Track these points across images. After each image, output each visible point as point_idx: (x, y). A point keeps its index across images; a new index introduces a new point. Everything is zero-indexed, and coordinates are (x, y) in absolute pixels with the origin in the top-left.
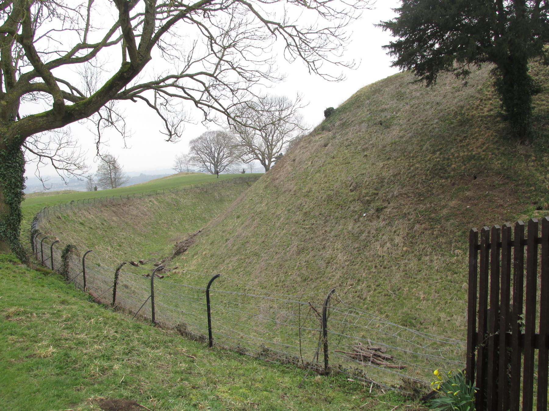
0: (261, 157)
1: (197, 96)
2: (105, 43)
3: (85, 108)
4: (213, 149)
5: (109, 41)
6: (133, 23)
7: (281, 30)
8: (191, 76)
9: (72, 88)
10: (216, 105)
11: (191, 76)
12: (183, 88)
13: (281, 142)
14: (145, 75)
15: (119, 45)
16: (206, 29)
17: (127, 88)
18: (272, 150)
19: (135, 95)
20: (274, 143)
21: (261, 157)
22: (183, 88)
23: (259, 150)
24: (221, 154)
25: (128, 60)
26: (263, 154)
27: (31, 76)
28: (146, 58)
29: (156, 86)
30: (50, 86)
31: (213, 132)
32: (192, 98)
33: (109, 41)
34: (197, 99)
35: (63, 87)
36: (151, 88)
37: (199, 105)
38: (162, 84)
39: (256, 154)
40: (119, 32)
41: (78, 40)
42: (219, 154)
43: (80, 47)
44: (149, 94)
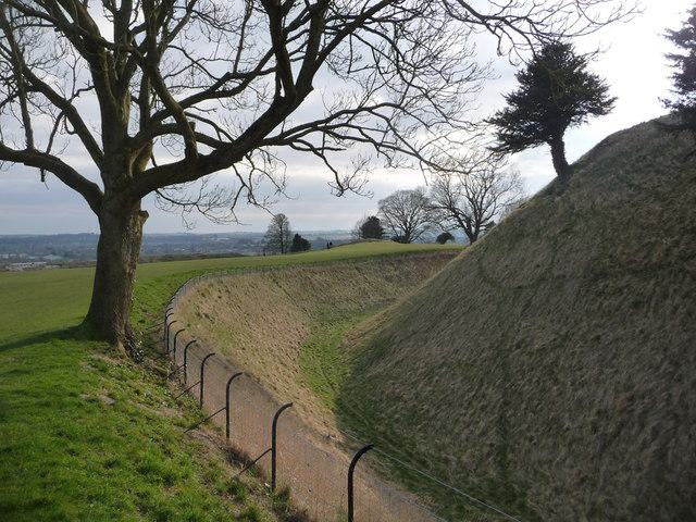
0: (465, 224)
1: (378, 137)
2: (258, 72)
3: (229, 153)
4: (406, 212)
5: (263, 70)
6: (290, 47)
7: (507, 28)
8: (370, 110)
9: (218, 130)
10: (406, 148)
11: (370, 110)
12: (360, 129)
13: (493, 205)
14: (310, 109)
15: (273, 74)
16: (299, 149)
17: (287, 129)
18: (481, 215)
19: (295, 139)
20: (484, 207)
21: (465, 224)
22: (360, 129)
23: (463, 215)
24: (415, 218)
25: (283, 94)
26: (469, 220)
27: (161, 115)
28: (305, 86)
29: (323, 126)
30: (184, 128)
31: (407, 192)
32: (370, 140)
33: (263, 70)
34: (378, 141)
35: (200, 128)
36: (316, 129)
37: (381, 149)
38: (334, 122)
39: (460, 220)
40: (272, 63)
41: (228, 68)
42: (412, 218)
43: (228, 77)
44: (315, 138)
